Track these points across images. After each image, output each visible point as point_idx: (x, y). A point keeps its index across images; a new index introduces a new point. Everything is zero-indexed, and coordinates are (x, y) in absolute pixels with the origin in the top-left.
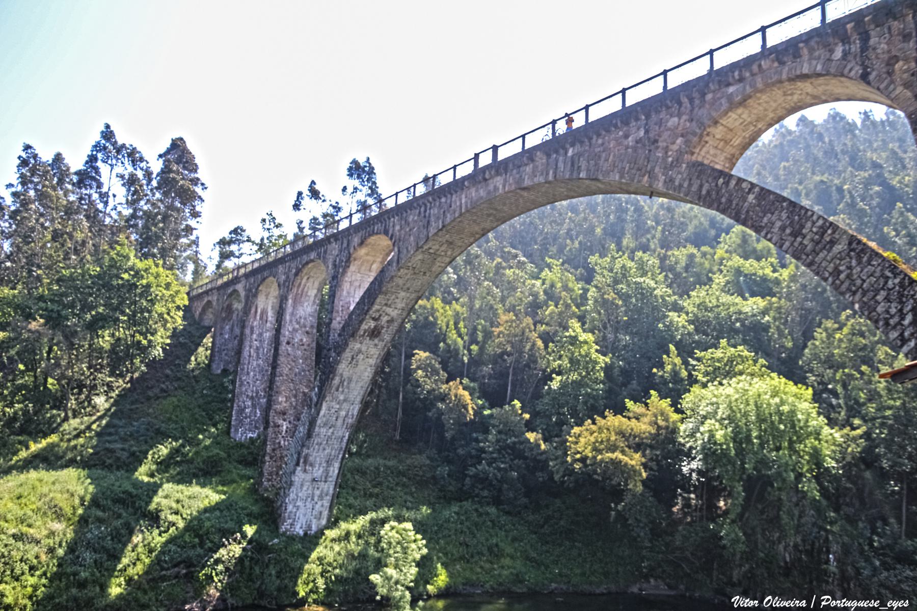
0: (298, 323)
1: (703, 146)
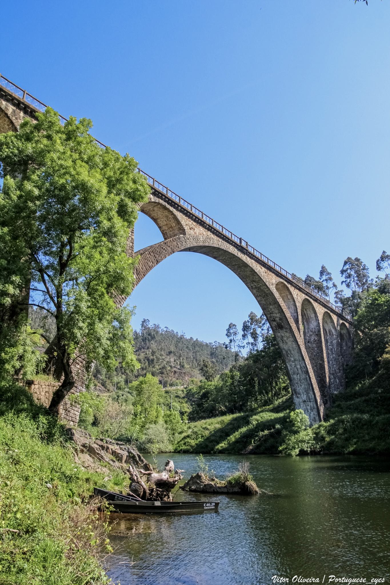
0: (312, 331)
1: (167, 234)
